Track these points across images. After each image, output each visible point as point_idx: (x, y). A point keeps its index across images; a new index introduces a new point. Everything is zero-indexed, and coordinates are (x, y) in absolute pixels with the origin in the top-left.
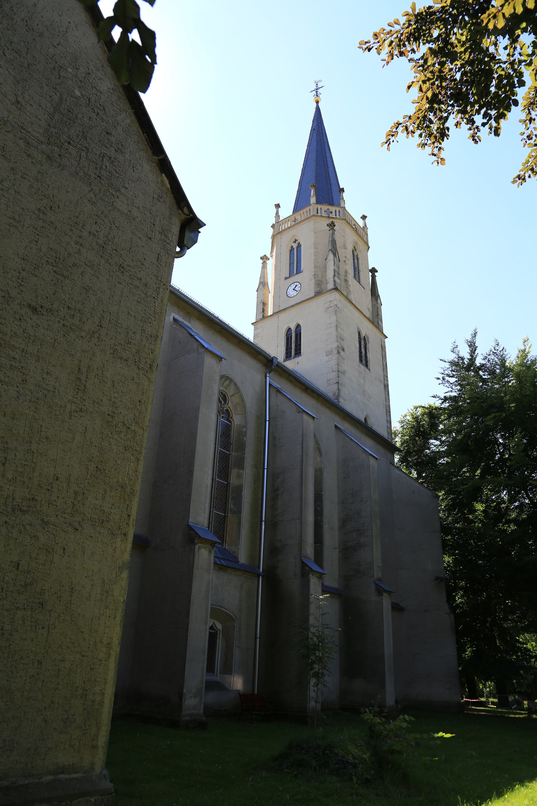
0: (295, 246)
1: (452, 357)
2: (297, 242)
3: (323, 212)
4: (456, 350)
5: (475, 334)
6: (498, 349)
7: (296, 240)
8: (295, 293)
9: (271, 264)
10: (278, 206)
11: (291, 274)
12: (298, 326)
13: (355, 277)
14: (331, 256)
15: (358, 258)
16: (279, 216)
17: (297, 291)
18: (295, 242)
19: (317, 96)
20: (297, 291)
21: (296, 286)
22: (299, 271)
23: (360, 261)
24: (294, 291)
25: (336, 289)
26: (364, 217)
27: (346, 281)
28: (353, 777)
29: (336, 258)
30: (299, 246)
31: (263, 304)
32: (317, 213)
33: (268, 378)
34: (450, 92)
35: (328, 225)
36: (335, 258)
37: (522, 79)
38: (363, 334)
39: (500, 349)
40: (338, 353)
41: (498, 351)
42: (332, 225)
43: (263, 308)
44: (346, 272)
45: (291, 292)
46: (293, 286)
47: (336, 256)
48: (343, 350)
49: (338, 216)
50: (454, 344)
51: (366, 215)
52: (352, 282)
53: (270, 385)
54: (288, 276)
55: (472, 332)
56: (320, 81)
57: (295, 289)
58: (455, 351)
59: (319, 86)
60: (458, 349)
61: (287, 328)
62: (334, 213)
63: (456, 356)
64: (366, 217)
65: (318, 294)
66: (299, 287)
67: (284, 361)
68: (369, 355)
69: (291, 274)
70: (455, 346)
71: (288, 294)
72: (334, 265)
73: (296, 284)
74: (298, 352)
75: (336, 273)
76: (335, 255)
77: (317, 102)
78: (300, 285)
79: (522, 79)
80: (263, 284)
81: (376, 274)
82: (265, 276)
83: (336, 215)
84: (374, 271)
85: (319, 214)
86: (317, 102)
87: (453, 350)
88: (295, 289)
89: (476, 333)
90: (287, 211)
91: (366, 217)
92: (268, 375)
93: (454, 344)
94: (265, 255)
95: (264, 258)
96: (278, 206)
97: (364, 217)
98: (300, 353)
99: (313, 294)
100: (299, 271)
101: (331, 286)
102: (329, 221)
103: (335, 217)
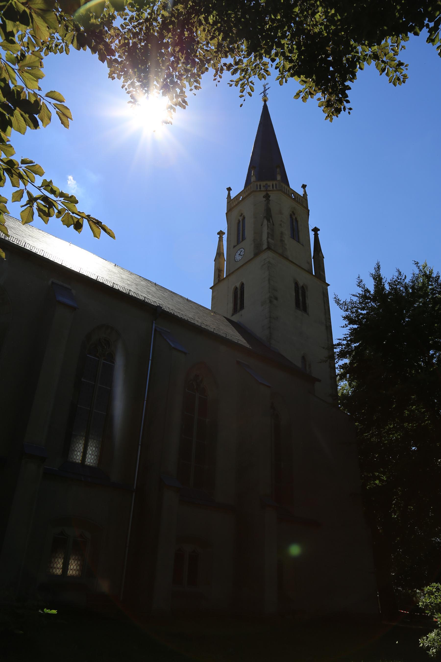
0: (241, 219)
1: (360, 291)
2: (242, 215)
4: (361, 284)
5: (379, 267)
6: (401, 278)
7: (242, 214)
8: (240, 257)
9: (225, 237)
10: (229, 189)
11: (238, 242)
12: (242, 285)
14: (265, 222)
15: (297, 221)
17: (242, 255)
18: (241, 216)
19: (265, 96)
20: (242, 255)
21: (241, 251)
23: (299, 223)
24: (240, 256)
25: (269, 248)
26: (304, 186)
27: (282, 241)
29: (270, 222)
30: (244, 218)
31: (218, 271)
33: (154, 324)
36: (269, 223)
38: (301, 284)
39: (403, 278)
40: (271, 302)
41: (402, 280)
42: (267, 197)
43: (218, 274)
44: (282, 233)
45: (238, 258)
46: (239, 252)
47: (270, 221)
48: (276, 299)
49: (275, 189)
50: (358, 279)
51: (305, 184)
52: (289, 242)
53: (155, 330)
54: (236, 244)
55: (374, 265)
56: (267, 84)
57: (240, 254)
58: (360, 285)
59: (267, 88)
60: (363, 283)
61: (234, 287)
62: (271, 187)
63: (362, 289)
64: (306, 186)
65: (256, 255)
66: (243, 252)
67: (233, 315)
68: (308, 302)
69: (238, 242)
70: (360, 281)
71: (235, 259)
72: (268, 229)
73: (241, 250)
74: (242, 307)
75: (271, 235)
76: (268, 220)
77: (265, 101)
78: (243, 249)
80: (219, 254)
82: (221, 247)
83: (273, 188)
84: (316, 230)
86: (265, 101)
87: (358, 284)
88: (240, 254)
89: (379, 266)
91: (306, 186)
92: (154, 322)
93: (358, 279)
94: (221, 231)
95: (221, 233)
96: (229, 189)
97: (304, 186)
98: (243, 307)
99: (252, 256)
101: (265, 246)
102: (264, 193)
103: (273, 189)
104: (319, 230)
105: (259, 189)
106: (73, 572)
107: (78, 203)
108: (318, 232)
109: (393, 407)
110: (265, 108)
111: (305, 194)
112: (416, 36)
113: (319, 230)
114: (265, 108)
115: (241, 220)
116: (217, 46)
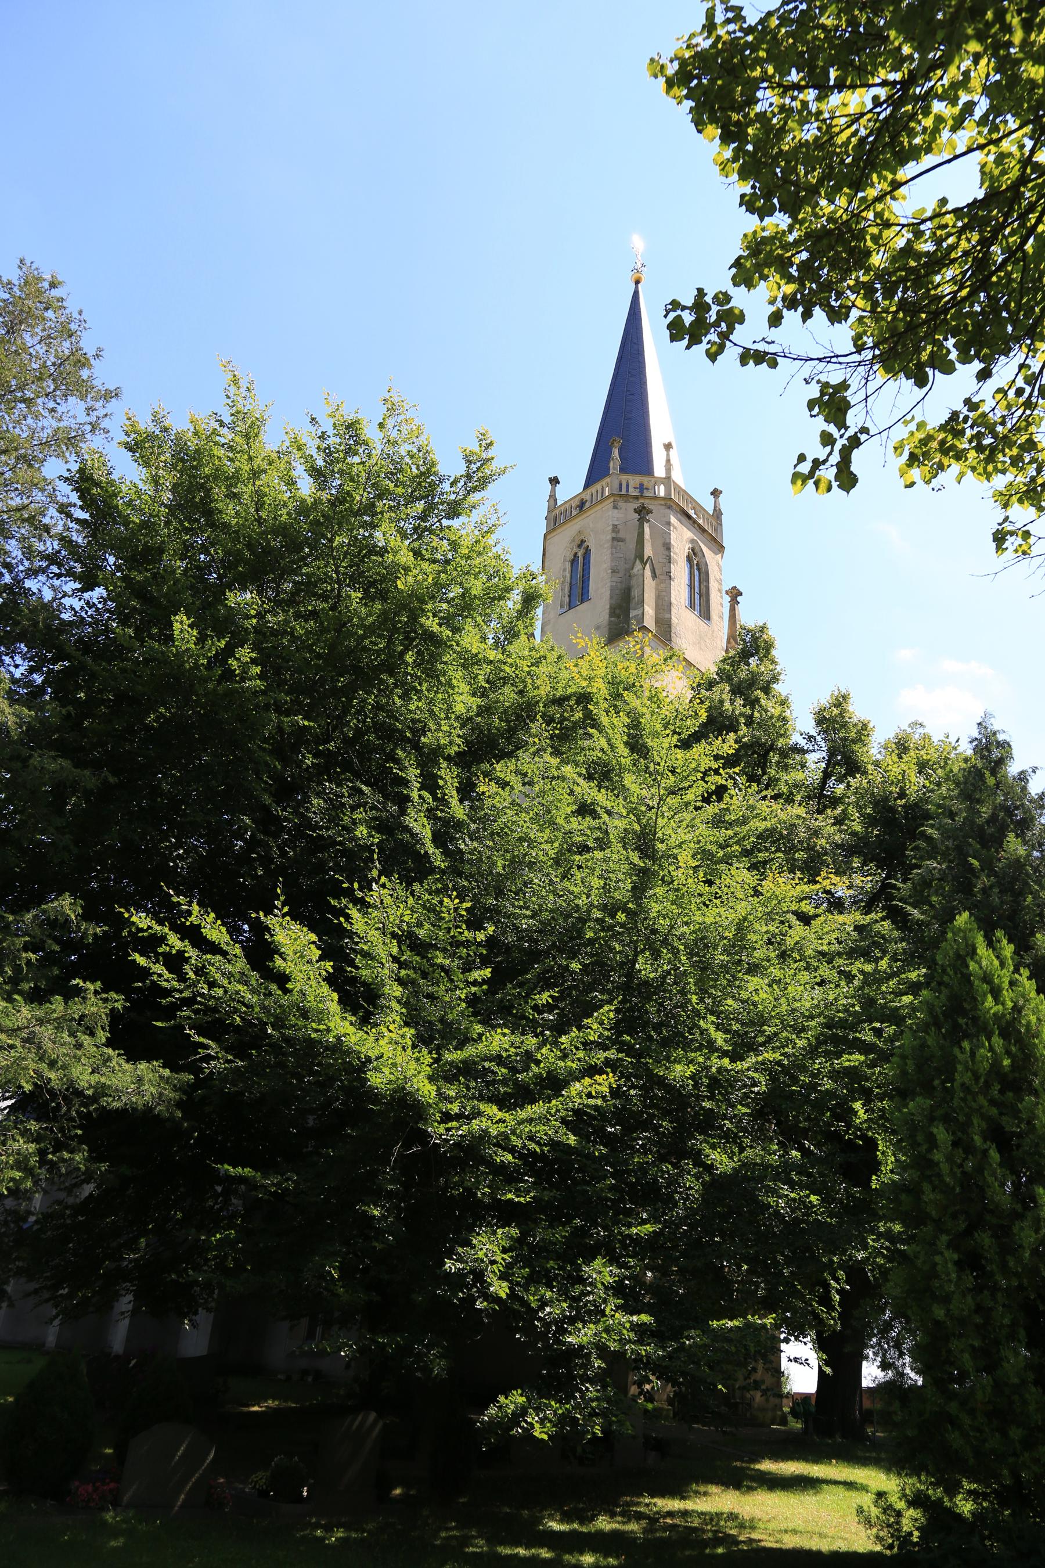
3: (631, 489)
7: (583, 542)
10: (554, 481)
13: (692, 605)
16: (556, 500)
18: (579, 546)
22: (584, 597)
26: (716, 493)
28: (74, 498)
32: (621, 490)
34: (795, 267)
35: (635, 511)
37: (687, 325)
51: (720, 489)
77: (637, 282)
79: (687, 325)
81: (739, 599)
85: (624, 492)
90: (572, 487)
96: (554, 481)
97: (716, 493)
100: (584, 597)
104: (741, 594)
105: (624, 492)
106: (867, 397)
107: (991, 537)
108: (739, 599)
109: (958, 1477)
110: (636, 295)
111: (718, 514)
112: (819, 439)
113: (741, 594)
114: (636, 295)
115: (580, 554)
116: (1009, 942)
